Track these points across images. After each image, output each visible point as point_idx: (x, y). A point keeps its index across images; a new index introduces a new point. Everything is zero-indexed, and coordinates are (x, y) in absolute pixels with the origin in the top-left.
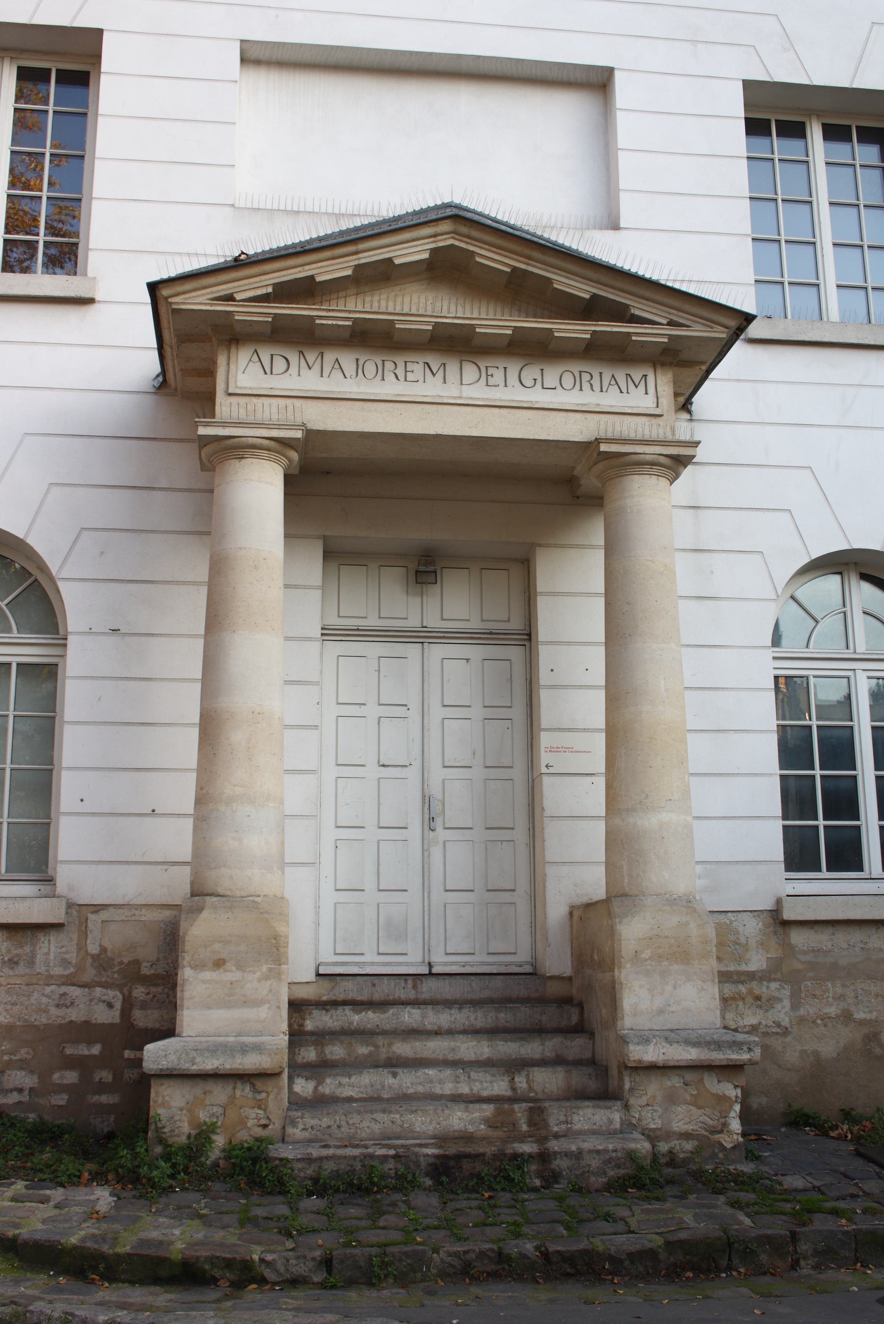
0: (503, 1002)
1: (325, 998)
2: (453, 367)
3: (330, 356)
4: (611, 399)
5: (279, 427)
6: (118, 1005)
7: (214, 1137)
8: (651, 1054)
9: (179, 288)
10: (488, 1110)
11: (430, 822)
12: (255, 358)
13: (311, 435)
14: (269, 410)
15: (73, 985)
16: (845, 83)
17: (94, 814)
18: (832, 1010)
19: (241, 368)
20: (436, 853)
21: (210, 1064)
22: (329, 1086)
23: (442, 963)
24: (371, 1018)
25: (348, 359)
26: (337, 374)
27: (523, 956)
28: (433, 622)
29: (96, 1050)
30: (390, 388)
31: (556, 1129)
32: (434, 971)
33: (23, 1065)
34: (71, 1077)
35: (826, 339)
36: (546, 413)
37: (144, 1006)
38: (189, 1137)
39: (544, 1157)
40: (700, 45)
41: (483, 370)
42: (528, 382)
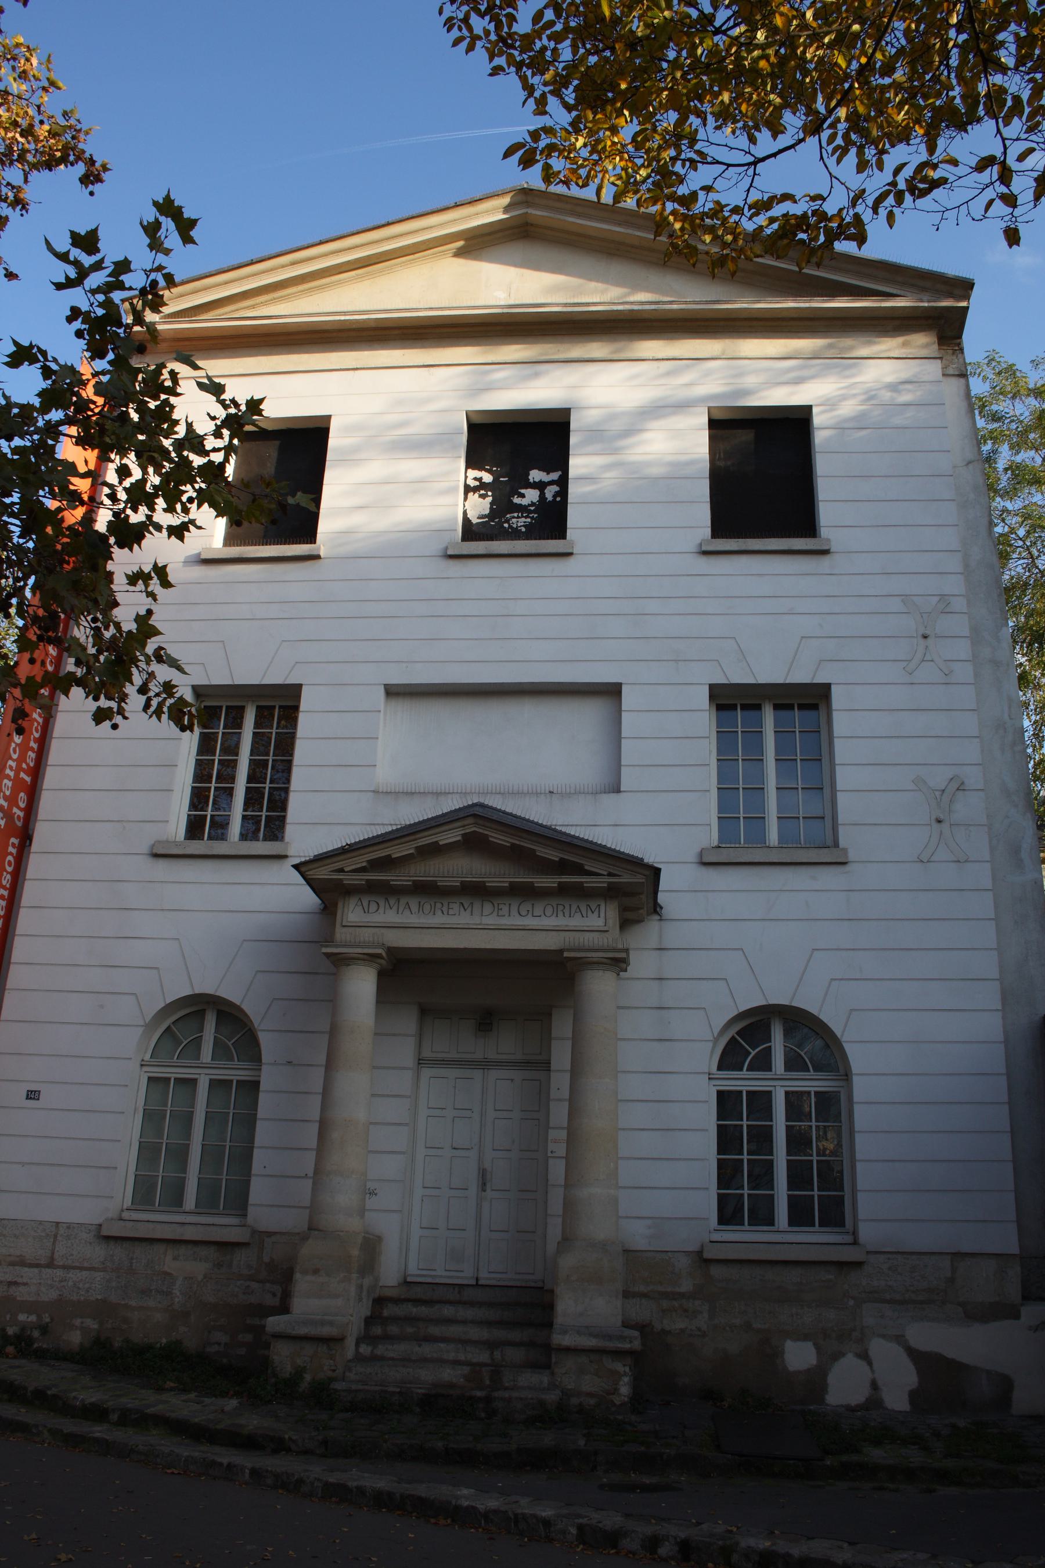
1: (403, 1297)
2: (477, 905)
3: (403, 901)
4: (576, 922)
5: (368, 947)
6: (279, 1295)
7: (305, 1375)
8: (567, 1340)
9: (311, 866)
10: (466, 1370)
11: (483, 1186)
12: (359, 903)
13: (390, 950)
14: (366, 935)
15: (253, 1281)
16: (779, 680)
17: (272, 1176)
19: (351, 909)
21: (303, 1331)
22: (380, 1350)
24: (423, 1311)
25: (414, 903)
26: (407, 912)
30: (439, 919)
31: (507, 1385)
32: (480, 1283)
34: (249, 1337)
35: (756, 861)
36: (534, 932)
38: (290, 1374)
39: (488, 1400)
40: (680, 663)
41: (496, 905)
42: (524, 913)
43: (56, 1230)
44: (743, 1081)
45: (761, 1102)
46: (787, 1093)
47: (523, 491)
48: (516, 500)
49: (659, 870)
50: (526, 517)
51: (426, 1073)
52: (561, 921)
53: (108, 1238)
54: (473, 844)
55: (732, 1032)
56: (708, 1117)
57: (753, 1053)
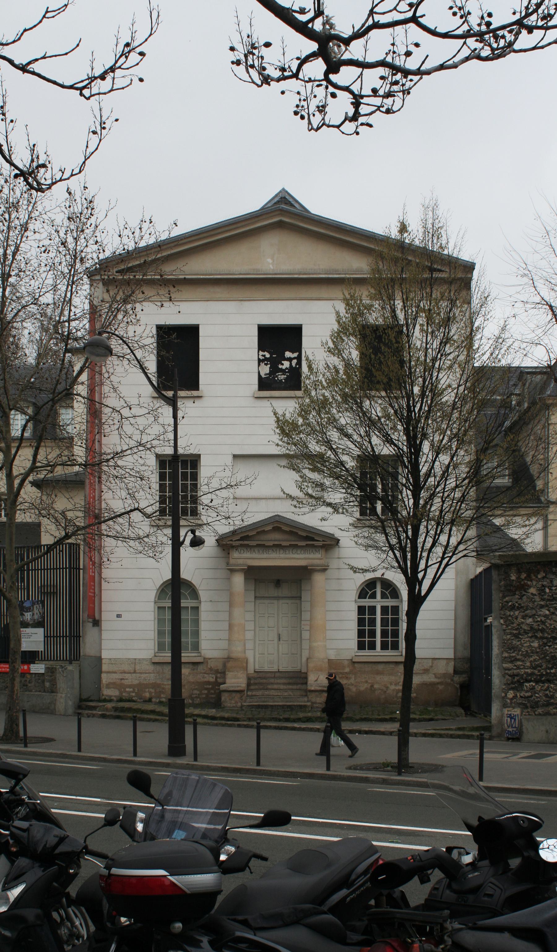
0: (291, 678)
4: (312, 556)
11: (279, 639)
14: (240, 561)
18: (363, 680)
20: (280, 646)
23: (281, 669)
27: (299, 668)
28: (280, 595)
29: (210, 686)
30: (265, 556)
33: (196, 689)
34: (206, 692)
37: (220, 678)
43: (135, 661)
44: (367, 602)
45: (372, 610)
46: (382, 607)
47: (283, 362)
48: (280, 366)
49: (339, 540)
50: (284, 375)
51: (258, 602)
52: (307, 556)
53: (154, 663)
54: (277, 529)
55: (363, 586)
56: (354, 616)
57: (370, 593)
